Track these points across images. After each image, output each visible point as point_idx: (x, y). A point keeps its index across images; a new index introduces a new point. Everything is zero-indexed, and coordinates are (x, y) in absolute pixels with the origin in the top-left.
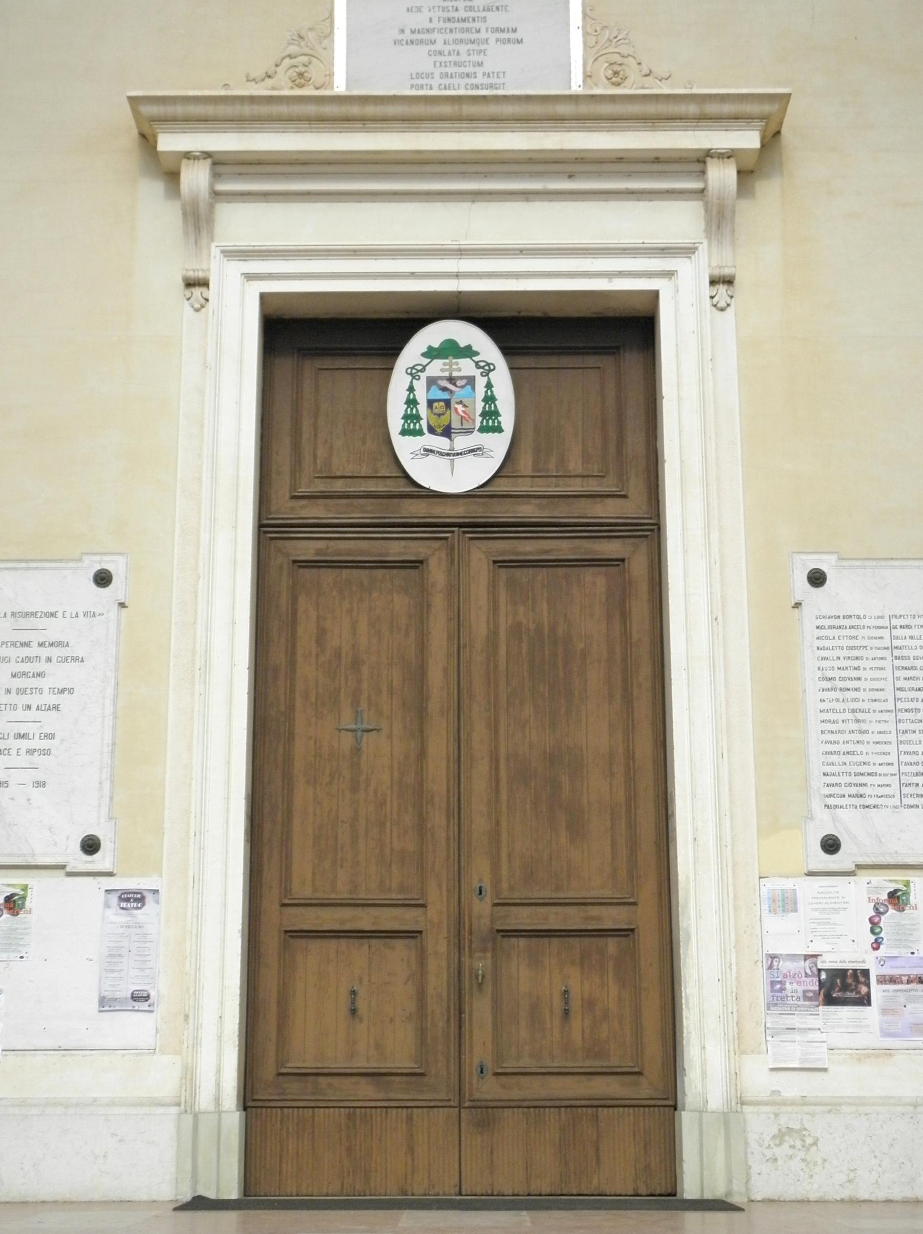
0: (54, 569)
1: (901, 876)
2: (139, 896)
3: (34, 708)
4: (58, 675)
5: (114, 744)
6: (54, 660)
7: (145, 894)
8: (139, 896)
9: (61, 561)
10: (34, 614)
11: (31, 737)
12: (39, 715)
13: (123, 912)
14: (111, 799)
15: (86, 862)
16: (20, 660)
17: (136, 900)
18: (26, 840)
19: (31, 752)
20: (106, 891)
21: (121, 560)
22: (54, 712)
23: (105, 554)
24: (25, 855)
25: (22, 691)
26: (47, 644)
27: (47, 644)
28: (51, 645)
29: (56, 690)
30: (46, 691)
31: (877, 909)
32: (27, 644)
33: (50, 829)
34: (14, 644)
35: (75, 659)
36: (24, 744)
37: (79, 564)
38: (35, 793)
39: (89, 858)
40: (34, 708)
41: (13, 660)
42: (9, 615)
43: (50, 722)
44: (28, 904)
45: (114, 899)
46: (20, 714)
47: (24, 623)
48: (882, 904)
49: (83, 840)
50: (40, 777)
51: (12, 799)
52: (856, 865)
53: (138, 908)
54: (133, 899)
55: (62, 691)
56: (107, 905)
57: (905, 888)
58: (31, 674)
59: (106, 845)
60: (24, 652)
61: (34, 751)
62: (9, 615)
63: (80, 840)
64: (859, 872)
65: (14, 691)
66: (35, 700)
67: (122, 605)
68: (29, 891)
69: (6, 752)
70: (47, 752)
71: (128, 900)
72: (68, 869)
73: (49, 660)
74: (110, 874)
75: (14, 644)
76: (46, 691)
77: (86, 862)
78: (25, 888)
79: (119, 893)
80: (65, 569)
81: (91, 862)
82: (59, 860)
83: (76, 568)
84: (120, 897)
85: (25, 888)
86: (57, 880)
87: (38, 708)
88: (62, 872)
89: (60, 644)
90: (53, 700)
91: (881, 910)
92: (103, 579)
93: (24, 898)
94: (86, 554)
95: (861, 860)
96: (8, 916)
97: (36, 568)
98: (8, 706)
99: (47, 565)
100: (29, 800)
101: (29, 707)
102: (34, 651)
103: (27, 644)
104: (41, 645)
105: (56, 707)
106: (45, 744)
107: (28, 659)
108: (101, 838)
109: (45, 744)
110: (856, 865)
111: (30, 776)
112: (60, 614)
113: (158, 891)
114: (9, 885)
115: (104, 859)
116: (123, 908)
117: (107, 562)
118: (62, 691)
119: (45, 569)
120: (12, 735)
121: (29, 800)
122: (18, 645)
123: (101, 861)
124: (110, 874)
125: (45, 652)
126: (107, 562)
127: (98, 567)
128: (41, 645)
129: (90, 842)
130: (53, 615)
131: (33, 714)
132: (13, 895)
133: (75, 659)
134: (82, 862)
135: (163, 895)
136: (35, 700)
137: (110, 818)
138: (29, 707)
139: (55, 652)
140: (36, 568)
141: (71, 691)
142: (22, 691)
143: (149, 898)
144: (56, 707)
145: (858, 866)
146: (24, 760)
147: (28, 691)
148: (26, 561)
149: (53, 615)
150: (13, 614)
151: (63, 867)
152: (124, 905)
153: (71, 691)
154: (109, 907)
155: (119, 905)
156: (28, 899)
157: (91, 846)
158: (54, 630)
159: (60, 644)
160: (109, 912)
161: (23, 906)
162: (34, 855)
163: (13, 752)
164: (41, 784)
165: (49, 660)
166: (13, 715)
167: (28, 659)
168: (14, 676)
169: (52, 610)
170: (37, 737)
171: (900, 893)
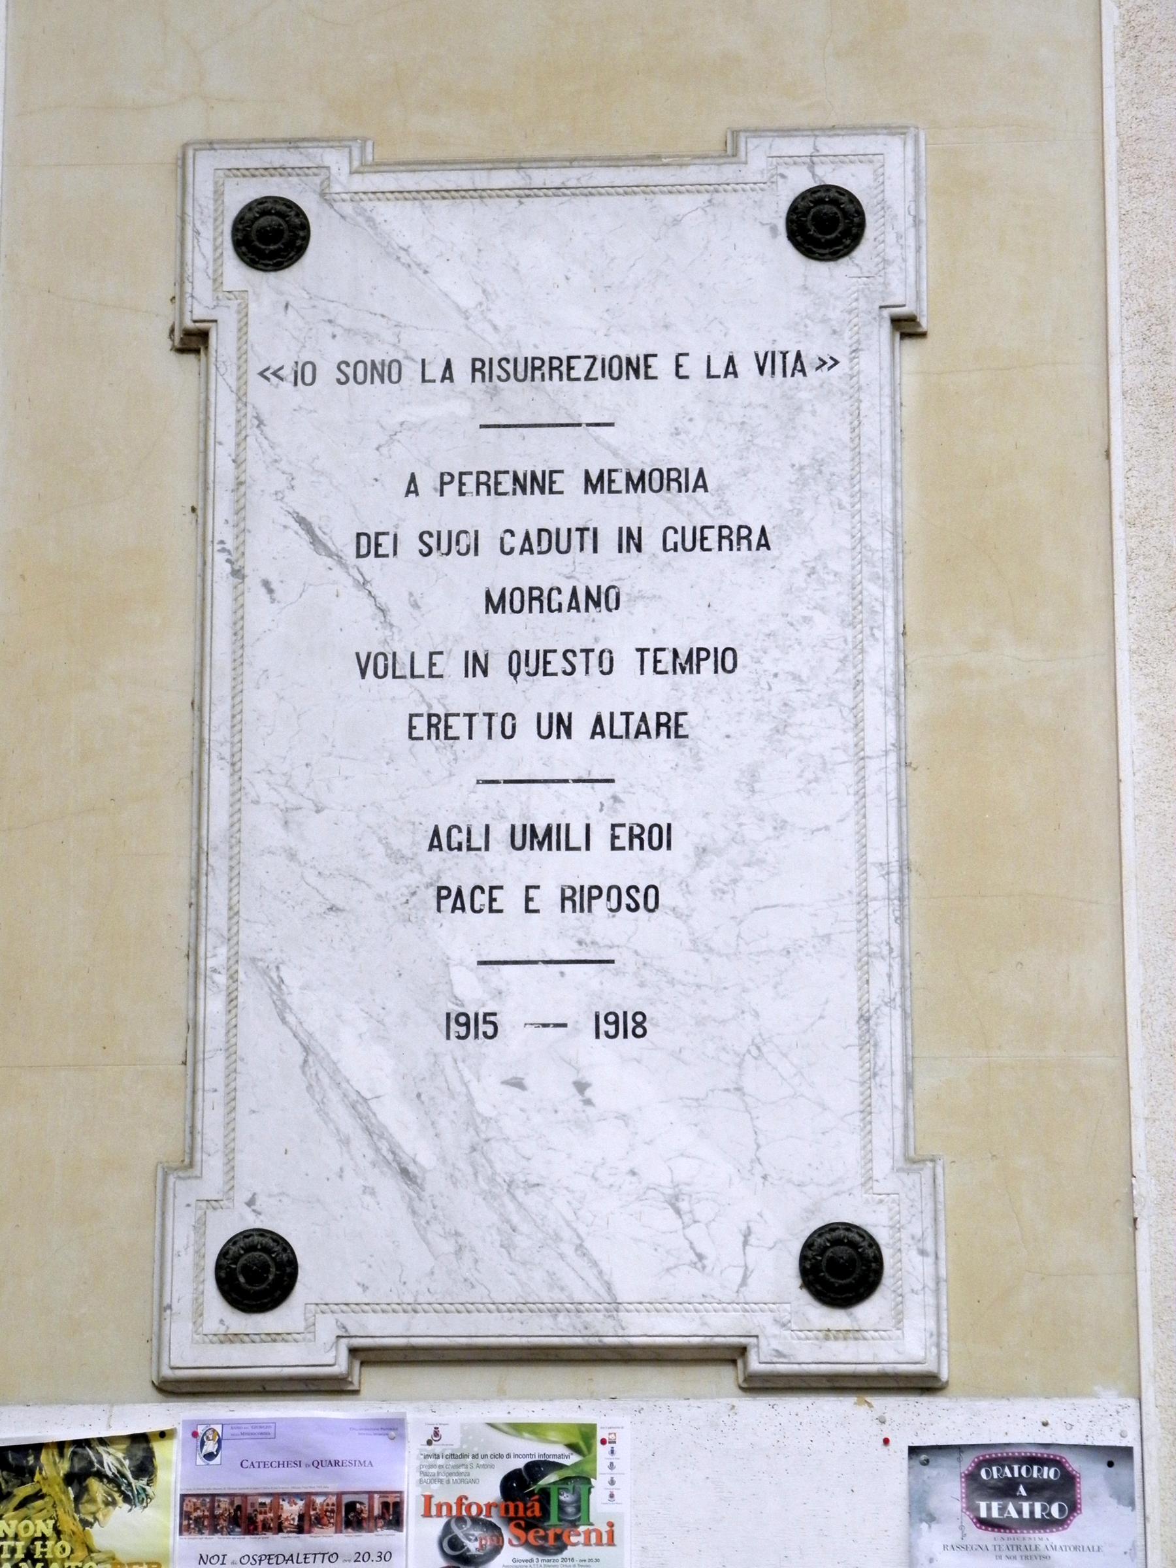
0: (629, 190)
1: (551, 1405)
2: (1049, 1473)
3: (582, 726)
4: (671, 600)
5: (905, 866)
6: (652, 541)
7: (1075, 1463)
8: (1049, 1473)
9: (654, 160)
10: (561, 367)
11: (577, 838)
12: (606, 755)
13: (989, 1537)
14: (909, 1084)
15: (828, 1334)
16: (517, 542)
17: (1036, 1489)
18: (580, 1248)
19: (577, 898)
20: (914, 1451)
21: (896, 154)
22: (662, 745)
23: (832, 130)
24: (578, 1307)
25: (529, 664)
26: (620, 481)
27: (620, 481)
28: (638, 482)
29: (666, 658)
30: (626, 660)
31: (455, 1543)
32: (538, 483)
33: (673, 1203)
34: (489, 483)
35: (733, 537)
36: (552, 870)
37: (729, 172)
38: (607, 1058)
39: (837, 1318)
40: (582, 726)
41: (488, 544)
42: (462, 370)
43: (649, 780)
44: (599, 1505)
45: (948, 1487)
46: (529, 752)
47: (520, 400)
48: (476, 1521)
49: (808, 1245)
50: (621, 995)
51: (518, 1084)
52: (353, 1351)
53: (1048, 1523)
54: (1028, 1486)
55: (690, 661)
56: (920, 1511)
57: (574, 1458)
58: (565, 598)
59: (903, 1265)
60: (534, 511)
61: (594, 893)
62: (462, 370)
63: (796, 1247)
64: (373, 1379)
65: (498, 665)
66: (582, 698)
67: (906, 327)
68: (601, 1451)
69: (481, 899)
70: (641, 899)
71: (1006, 1490)
72: (755, 1364)
73: (631, 540)
74: (924, 1385)
75: (489, 483)
76: (626, 660)
77: (828, 1334)
78: (583, 1440)
79: (968, 1462)
80: (674, 190)
81: (845, 1335)
82: (720, 1326)
83: (715, 188)
84: (972, 1478)
85: (583, 1440)
86: (707, 1409)
87: (598, 727)
88: (727, 1376)
89: (670, 480)
90: (655, 694)
91: (472, 1547)
92: (825, 225)
93: (581, 1480)
94: (757, 132)
95: (385, 1329)
96: (523, 1553)
97: (558, 190)
98: (480, 724)
99: (603, 176)
100: (581, 1087)
101: (562, 725)
102: (568, 508)
103: (538, 483)
104: (595, 483)
105: (670, 725)
106: (634, 867)
107: (547, 541)
108: (882, 1237)
109: (634, 867)
110: (353, 1351)
111: (579, 994)
112: (662, 366)
113: (1127, 1452)
114: (517, 1429)
115: (899, 1319)
116: (986, 1524)
117: (840, 159)
118: (690, 661)
119: (590, 191)
120: (500, 834)
121: (581, 1087)
122: (507, 483)
123: (889, 1328)
124: (924, 1385)
125: (612, 513)
126: (840, 159)
127: (801, 181)
128: (595, 483)
129: (843, 1252)
130: (636, 368)
131: (577, 753)
132: (536, 1469)
133: (733, 537)
134: (807, 1334)
135: (1154, 1468)
136: (582, 698)
137: (912, 1161)
138: (562, 725)
139: (654, 512)
140: (558, 190)
141: (724, 660)
142: (529, 664)
143: (1092, 1480)
144: (670, 725)
145: (367, 1356)
146: (553, 931)
147: (557, 663)
148: (518, 164)
149: (636, 368)
150: (478, 368)
151: (731, 1355)
152: (991, 1508)
153: (724, 660)
154: (931, 1519)
155: (972, 1509)
156: (600, 1486)
157: (841, 1267)
158: (644, 424)
159: (670, 480)
160: (932, 1539)
161: (578, 1514)
162: (614, 1306)
163: (511, 899)
164: (625, 1025)
165: (631, 540)
166: (501, 757)
167: (547, 541)
168: (495, 603)
169: (632, 348)
170: (600, 838)
171: (551, 1478)
